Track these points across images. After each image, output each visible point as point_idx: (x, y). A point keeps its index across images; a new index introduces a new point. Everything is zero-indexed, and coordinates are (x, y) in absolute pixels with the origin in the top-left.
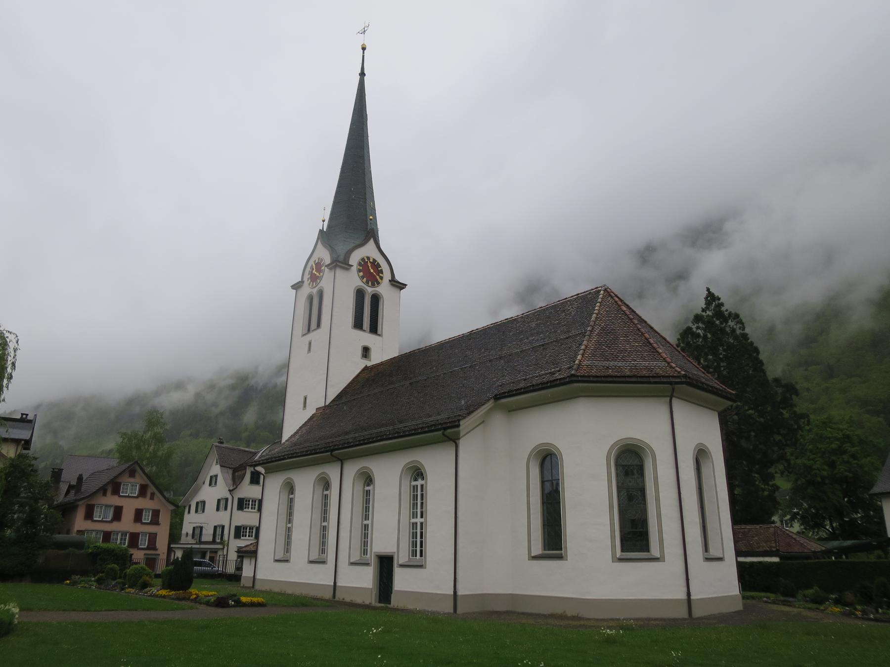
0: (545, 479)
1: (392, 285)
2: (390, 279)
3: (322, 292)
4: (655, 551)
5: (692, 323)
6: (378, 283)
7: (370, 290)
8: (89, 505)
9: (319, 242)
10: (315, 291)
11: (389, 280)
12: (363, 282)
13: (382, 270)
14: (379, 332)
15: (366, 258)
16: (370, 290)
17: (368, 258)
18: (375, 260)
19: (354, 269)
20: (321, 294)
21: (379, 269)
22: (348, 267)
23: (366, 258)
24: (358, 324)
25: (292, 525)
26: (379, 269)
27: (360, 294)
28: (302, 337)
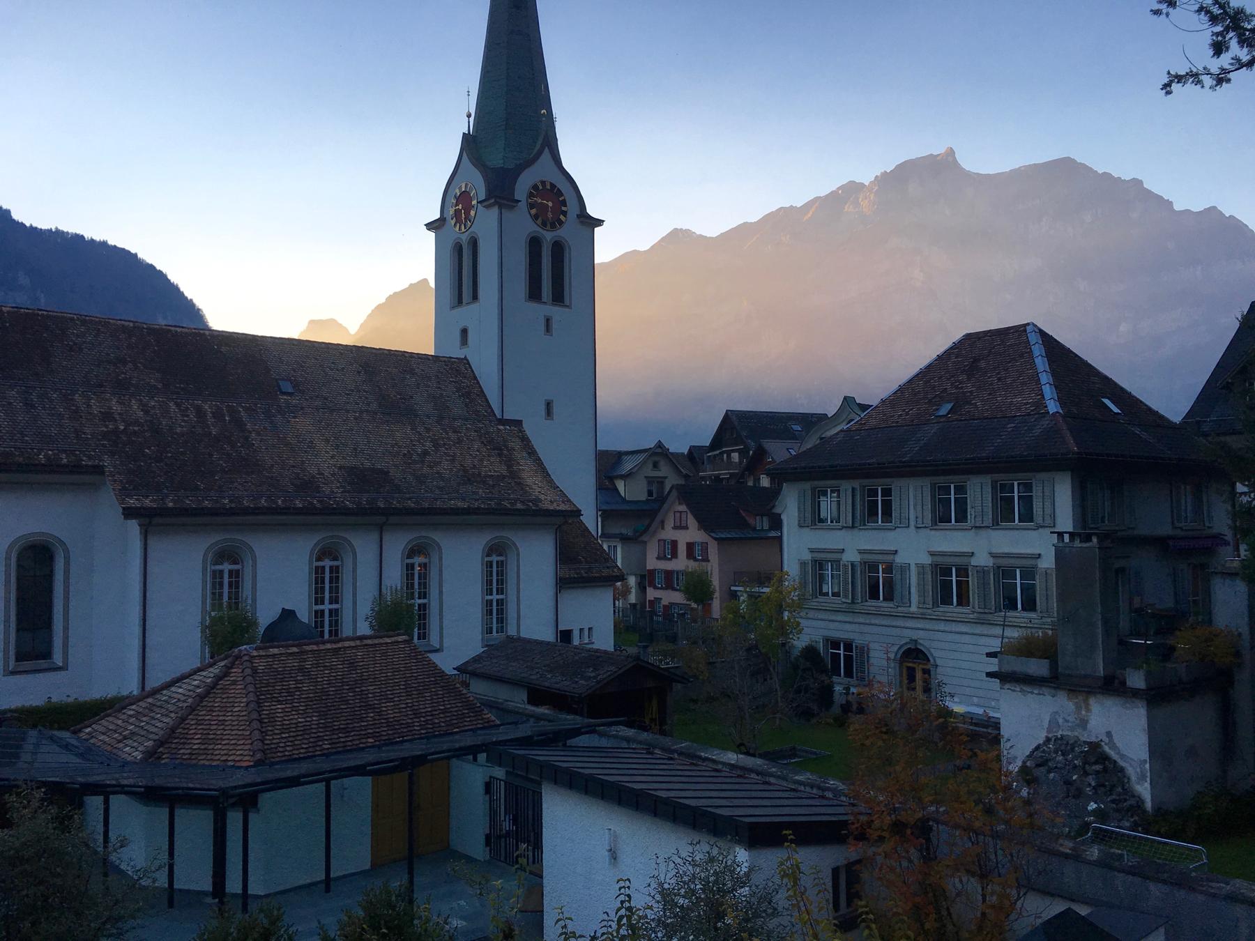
0: (1005, 628)
1: (582, 223)
2: (579, 213)
3: (476, 239)
4: (58, 658)
5: (841, 723)
6: (561, 223)
7: (548, 236)
8: (528, 702)
9: (465, 154)
10: (464, 238)
11: (577, 215)
12: (530, 213)
13: (564, 200)
14: (567, 301)
15: (539, 184)
16: (548, 236)
17: (543, 183)
18: (553, 186)
19: (523, 205)
20: (474, 243)
21: (561, 199)
22: (515, 204)
23: (539, 184)
24: (534, 294)
25: (429, 601)
26: (561, 199)
27: (535, 244)
28: (451, 310)
